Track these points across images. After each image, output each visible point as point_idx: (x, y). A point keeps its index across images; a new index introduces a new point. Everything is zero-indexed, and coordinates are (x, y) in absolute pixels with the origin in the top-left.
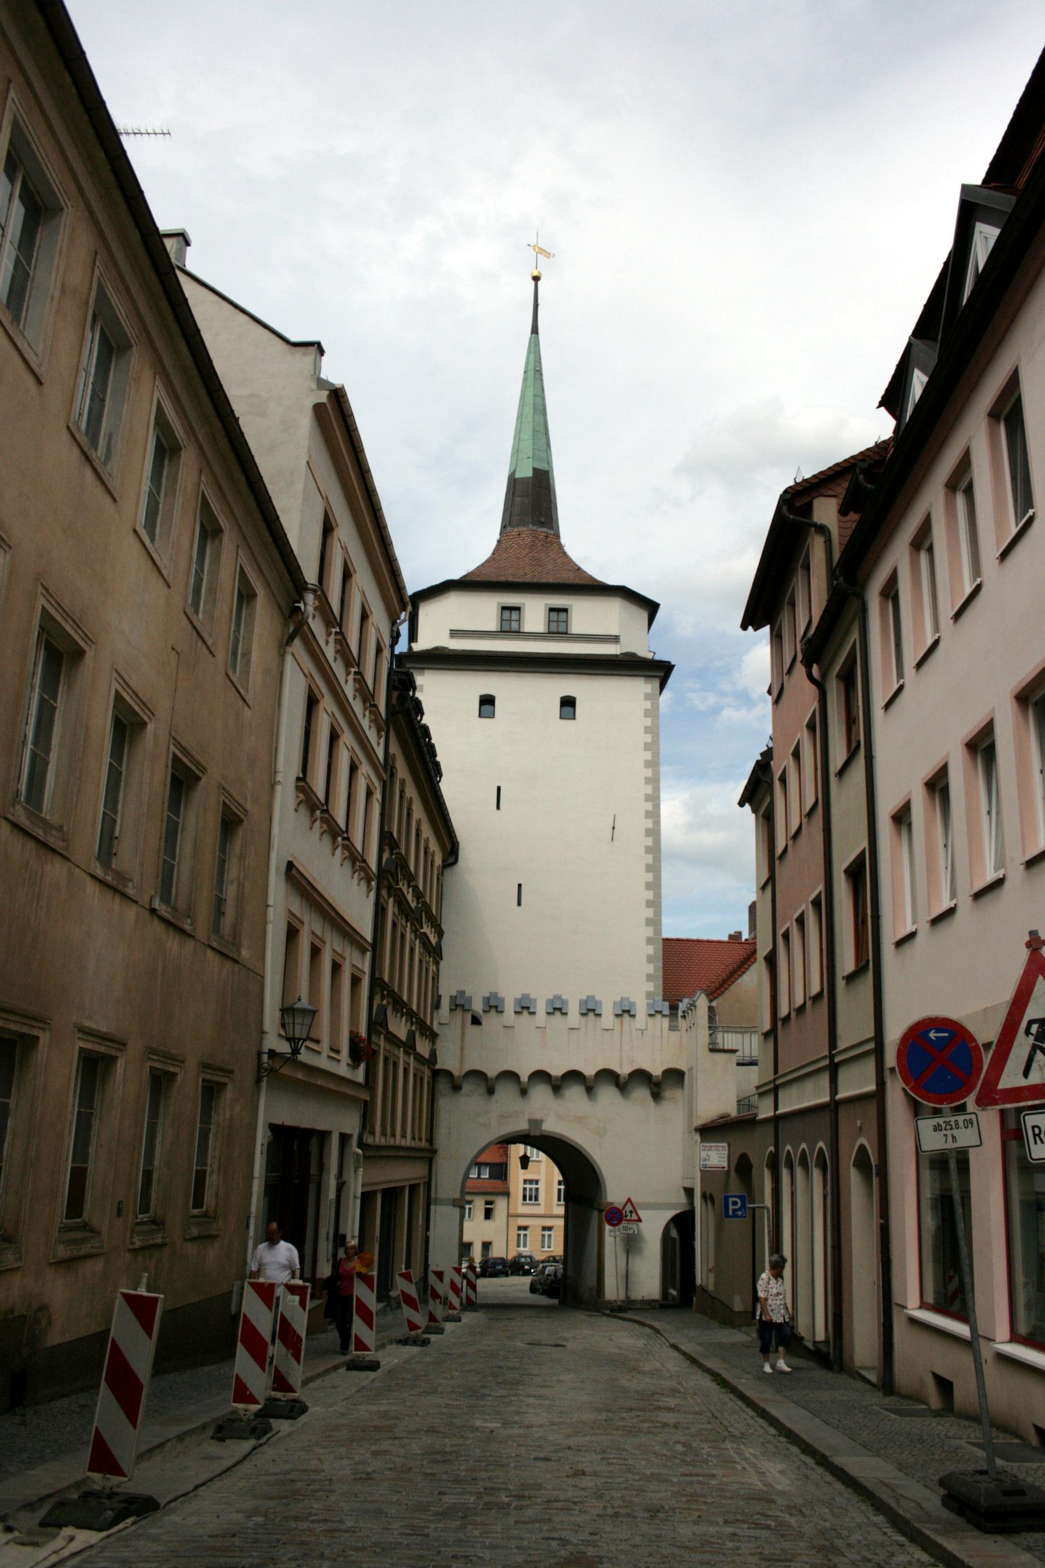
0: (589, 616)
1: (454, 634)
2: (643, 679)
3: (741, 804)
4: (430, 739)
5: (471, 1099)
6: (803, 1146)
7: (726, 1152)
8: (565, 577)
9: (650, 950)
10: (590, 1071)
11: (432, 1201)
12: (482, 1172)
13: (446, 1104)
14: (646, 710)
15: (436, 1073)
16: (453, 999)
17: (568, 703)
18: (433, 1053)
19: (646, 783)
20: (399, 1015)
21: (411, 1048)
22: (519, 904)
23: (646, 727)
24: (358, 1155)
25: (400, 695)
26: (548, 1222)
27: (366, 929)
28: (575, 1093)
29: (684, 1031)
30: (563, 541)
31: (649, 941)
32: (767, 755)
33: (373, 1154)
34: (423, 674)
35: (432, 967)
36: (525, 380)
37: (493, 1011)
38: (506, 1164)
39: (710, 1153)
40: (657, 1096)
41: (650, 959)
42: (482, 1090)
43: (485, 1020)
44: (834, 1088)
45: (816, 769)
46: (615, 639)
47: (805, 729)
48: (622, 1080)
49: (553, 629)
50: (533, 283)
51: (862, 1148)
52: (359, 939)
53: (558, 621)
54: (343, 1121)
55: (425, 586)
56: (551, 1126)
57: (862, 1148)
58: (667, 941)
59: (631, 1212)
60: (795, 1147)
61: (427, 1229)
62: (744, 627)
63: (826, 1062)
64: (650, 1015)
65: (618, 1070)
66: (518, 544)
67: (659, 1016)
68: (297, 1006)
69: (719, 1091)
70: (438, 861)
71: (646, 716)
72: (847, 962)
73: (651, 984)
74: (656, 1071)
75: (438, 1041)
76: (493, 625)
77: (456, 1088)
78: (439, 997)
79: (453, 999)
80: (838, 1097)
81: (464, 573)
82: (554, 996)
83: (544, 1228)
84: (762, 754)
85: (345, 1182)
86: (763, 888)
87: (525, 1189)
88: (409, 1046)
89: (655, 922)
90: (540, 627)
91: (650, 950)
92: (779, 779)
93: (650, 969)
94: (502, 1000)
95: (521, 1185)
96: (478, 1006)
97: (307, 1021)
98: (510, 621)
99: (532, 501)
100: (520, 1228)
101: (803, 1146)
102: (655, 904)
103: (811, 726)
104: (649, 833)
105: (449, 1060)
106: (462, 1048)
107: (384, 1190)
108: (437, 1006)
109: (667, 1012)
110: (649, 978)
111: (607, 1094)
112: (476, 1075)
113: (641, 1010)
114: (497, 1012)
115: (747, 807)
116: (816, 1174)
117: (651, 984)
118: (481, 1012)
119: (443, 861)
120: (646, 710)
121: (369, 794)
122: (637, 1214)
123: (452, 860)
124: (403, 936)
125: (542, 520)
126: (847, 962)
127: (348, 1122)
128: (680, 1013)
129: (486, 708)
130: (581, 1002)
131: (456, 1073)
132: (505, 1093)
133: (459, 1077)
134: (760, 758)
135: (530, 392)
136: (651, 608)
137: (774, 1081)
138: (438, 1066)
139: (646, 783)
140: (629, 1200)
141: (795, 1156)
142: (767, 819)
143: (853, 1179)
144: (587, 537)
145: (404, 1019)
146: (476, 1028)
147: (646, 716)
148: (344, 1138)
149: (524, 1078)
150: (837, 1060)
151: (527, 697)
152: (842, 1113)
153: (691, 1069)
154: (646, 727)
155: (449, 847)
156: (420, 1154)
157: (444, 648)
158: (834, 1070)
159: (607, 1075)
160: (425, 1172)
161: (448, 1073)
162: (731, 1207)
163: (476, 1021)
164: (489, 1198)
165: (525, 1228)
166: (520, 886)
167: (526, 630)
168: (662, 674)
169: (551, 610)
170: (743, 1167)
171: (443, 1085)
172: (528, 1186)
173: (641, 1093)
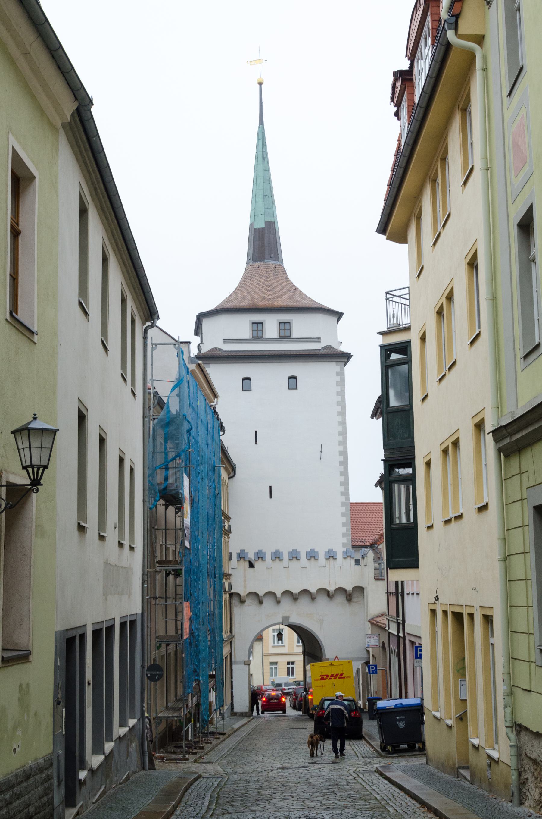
0: (302, 326)
1: (225, 341)
2: (334, 364)
3: (376, 486)
5: (250, 607)
10: (313, 590)
11: (233, 663)
13: (237, 611)
15: (231, 595)
19: (342, 516)
23: (337, 392)
26: (291, 659)
28: (304, 601)
31: (343, 504)
34: (209, 367)
36: (257, 158)
37: (260, 559)
41: (344, 525)
42: (256, 602)
43: (256, 564)
45: (522, 57)
46: (318, 340)
48: (331, 594)
49: (282, 334)
58: (354, 505)
61: (232, 677)
62: (372, 417)
66: (259, 274)
67: (349, 559)
68: (31, 426)
73: (344, 508)
74: (349, 588)
77: (242, 602)
78: (231, 553)
82: (293, 550)
83: (288, 663)
87: (288, 668)
89: (346, 494)
91: (343, 509)
93: (344, 530)
97: (47, 443)
98: (258, 334)
99: (264, 244)
100: (271, 663)
102: (345, 484)
104: (340, 434)
106: (245, 580)
110: (344, 535)
111: (322, 600)
113: (340, 556)
117: (344, 508)
123: (232, 475)
131: (242, 594)
132: (268, 603)
133: (244, 596)
135: (260, 167)
138: (232, 591)
139: (342, 516)
140: (336, 657)
146: (252, 569)
149: (279, 595)
154: (337, 392)
159: (323, 591)
161: (238, 595)
162: (371, 670)
163: (251, 565)
165: (276, 663)
167: (267, 338)
171: (235, 601)
173: (340, 599)
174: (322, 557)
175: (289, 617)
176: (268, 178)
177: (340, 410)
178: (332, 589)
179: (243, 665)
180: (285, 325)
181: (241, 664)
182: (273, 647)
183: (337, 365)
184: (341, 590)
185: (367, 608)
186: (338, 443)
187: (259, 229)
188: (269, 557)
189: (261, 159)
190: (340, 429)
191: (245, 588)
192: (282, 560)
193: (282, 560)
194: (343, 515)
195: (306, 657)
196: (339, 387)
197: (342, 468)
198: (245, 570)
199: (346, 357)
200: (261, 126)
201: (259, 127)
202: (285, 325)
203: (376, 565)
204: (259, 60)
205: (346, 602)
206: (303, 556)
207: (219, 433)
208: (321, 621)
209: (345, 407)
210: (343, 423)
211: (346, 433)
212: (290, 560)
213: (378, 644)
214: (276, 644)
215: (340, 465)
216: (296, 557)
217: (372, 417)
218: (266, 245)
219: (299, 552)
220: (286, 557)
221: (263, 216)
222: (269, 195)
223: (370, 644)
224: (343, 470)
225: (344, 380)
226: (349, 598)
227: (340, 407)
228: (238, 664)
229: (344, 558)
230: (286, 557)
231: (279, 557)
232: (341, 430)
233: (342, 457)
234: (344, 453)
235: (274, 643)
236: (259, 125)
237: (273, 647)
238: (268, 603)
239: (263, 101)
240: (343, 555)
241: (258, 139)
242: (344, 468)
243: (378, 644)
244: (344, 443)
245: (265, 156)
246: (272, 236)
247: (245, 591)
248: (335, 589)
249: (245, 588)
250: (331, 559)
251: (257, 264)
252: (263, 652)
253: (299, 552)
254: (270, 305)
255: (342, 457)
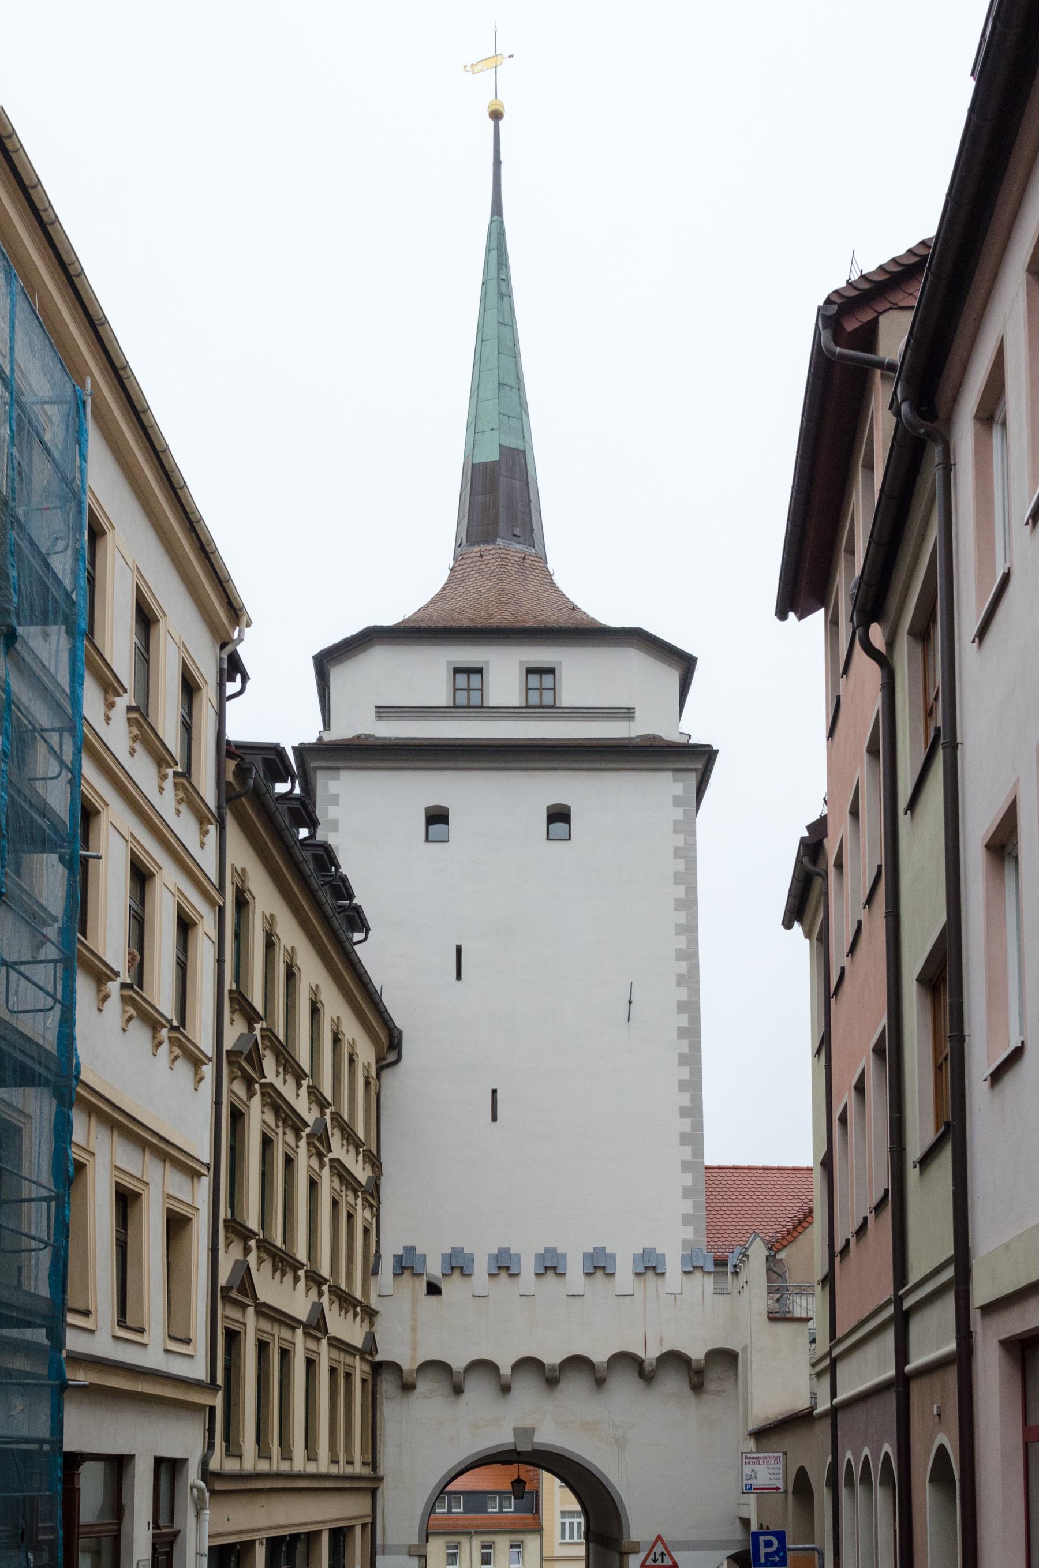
0: (585, 678)
1: (383, 712)
2: (669, 775)
3: (788, 924)
4: (338, 867)
6: (866, 1451)
7: (781, 1466)
8: (553, 618)
9: (688, 1179)
10: (600, 1356)
12: (505, 1504)
13: (394, 1412)
14: (676, 822)
15: (378, 1368)
16: (398, 1259)
17: (559, 815)
18: (371, 1339)
20: (350, 1314)
21: (317, 1328)
22: (494, 1118)
24: (200, 1490)
25: (238, 767)
27: (199, 1144)
28: (575, 1387)
29: (736, 1294)
30: (551, 567)
31: (686, 1166)
32: (819, 829)
33: (221, 1486)
35: (362, 1215)
37: (457, 1272)
38: (537, 1492)
39: (756, 1467)
40: (697, 1387)
42: (447, 1389)
44: (902, 1354)
46: (627, 713)
47: (853, 1090)
48: (647, 1368)
50: (492, 123)
51: (942, 1448)
52: (176, 1154)
53: (541, 689)
54: (183, 1440)
55: (336, 639)
56: (549, 1436)
57: (942, 1448)
59: (662, 1554)
60: (857, 1454)
62: (782, 614)
63: (890, 1311)
64: (686, 1273)
65: (640, 1353)
67: (698, 1274)
69: (780, 1377)
70: (367, 1055)
71: (676, 831)
72: (920, 1133)
74: (697, 1353)
75: (379, 1320)
76: (441, 697)
77: (408, 1387)
79: (398, 1259)
80: (908, 1368)
81: (401, 619)
82: (547, 1250)
84: (809, 828)
85: (177, 1534)
86: (818, 1052)
87: (563, 1524)
88: (316, 1326)
89: (694, 1139)
90: (515, 699)
92: (835, 865)
94: (471, 1257)
95: (558, 1520)
96: (434, 1268)
99: (499, 500)
101: (866, 1451)
102: (694, 1112)
103: (873, 750)
105: (393, 1348)
106: (414, 1329)
107: (267, 1539)
108: (372, 1270)
109: (710, 1267)
110: (687, 1220)
111: (624, 1388)
112: (436, 1367)
113: (673, 1267)
114: (463, 1275)
115: (797, 927)
116: (880, 1494)
118: (440, 1275)
119: (378, 1061)
120: (676, 822)
121: (185, 925)
122: (672, 1558)
124: (289, 1162)
125: (518, 531)
126: (920, 1133)
127: (183, 1440)
128: (730, 1269)
129: (436, 829)
130: (586, 1256)
132: (477, 1390)
133: (411, 1372)
134: (806, 834)
135: (492, 316)
136: (684, 664)
137: (830, 1353)
138: (378, 1358)
140: (659, 1538)
141: (857, 1464)
142: (821, 940)
143: (925, 1496)
144: (587, 565)
145: (359, 1318)
146: (433, 1299)
147: (676, 831)
148: (168, 1469)
149: (505, 1370)
150: (907, 1304)
151: (496, 806)
152: (915, 1388)
153: (744, 1349)
155: (384, 1038)
156: (362, 1484)
157: (368, 737)
158: (902, 1321)
159: (624, 1360)
160: (368, 1510)
161: (395, 1367)
162: (763, 1550)
163: (433, 1289)
164: (487, 1539)
166: (494, 1092)
168: (700, 766)
169: (530, 671)
170: (802, 1486)
171: (388, 1385)
172: (567, 1521)
173: (673, 1384)
174: (624, 1269)
175: (533, 1430)
176: (511, 344)
177: (686, 1024)
178: (651, 1354)
179: (407, 1557)
180: (540, 672)
181: (399, 1553)
182: (562, 1544)
183: (675, 780)
184: (674, 1359)
185: (745, 1399)
186: (674, 980)
187: (485, 464)
188: (481, 1268)
189: (493, 296)
190: (682, 942)
191: (414, 1349)
192: (517, 1275)
193: (517, 1275)
194: (687, 1193)
195: (591, 1545)
196: (681, 836)
197: (684, 1046)
198: (415, 1301)
199: (697, 760)
200: (495, 218)
201: (492, 222)
202: (540, 672)
203: (770, 1302)
204: (494, 61)
205: (687, 1390)
206: (575, 1268)
207: (221, 687)
208: (620, 1443)
209: (695, 888)
210: (690, 929)
211: (696, 955)
212: (537, 1275)
213: (780, 1484)
214: (567, 1540)
215: (679, 1037)
216: (555, 1268)
217: (782, 615)
218: (502, 502)
219: (564, 1256)
220: (527, 1267)
221: (496, 432)
222: (513, 383)
223: (755, 1483)
224: (686, 1051)
225: (699, 1049)
226: (696, 1380)
227: (682, 861)
228: (390, 1554)
229: (686, 1273)
230: (527, 1267)
231: (508, 1268)
232: (683, 945)
233: (688, 1095)
234: (691, 1008)
235: (563, 1538)
236: (492, 216)
237: (562, 1544)
238: (477, 1390)
239: (502, 158)
240: (683, 1264)
241: (489, 250)
242: (693, 1152)
243: (780, 1484)
244: (690, 979)
245: (504, 291)
246: (517, 484)
247: (413, 1358)
248: (658, 1354)
249: (414, 1349)
250: (650, 1273)
251: (477, 549)
252: (541, 1554)
253: (564, 1256)
254: (514, 670)
255: (688, 1095)
